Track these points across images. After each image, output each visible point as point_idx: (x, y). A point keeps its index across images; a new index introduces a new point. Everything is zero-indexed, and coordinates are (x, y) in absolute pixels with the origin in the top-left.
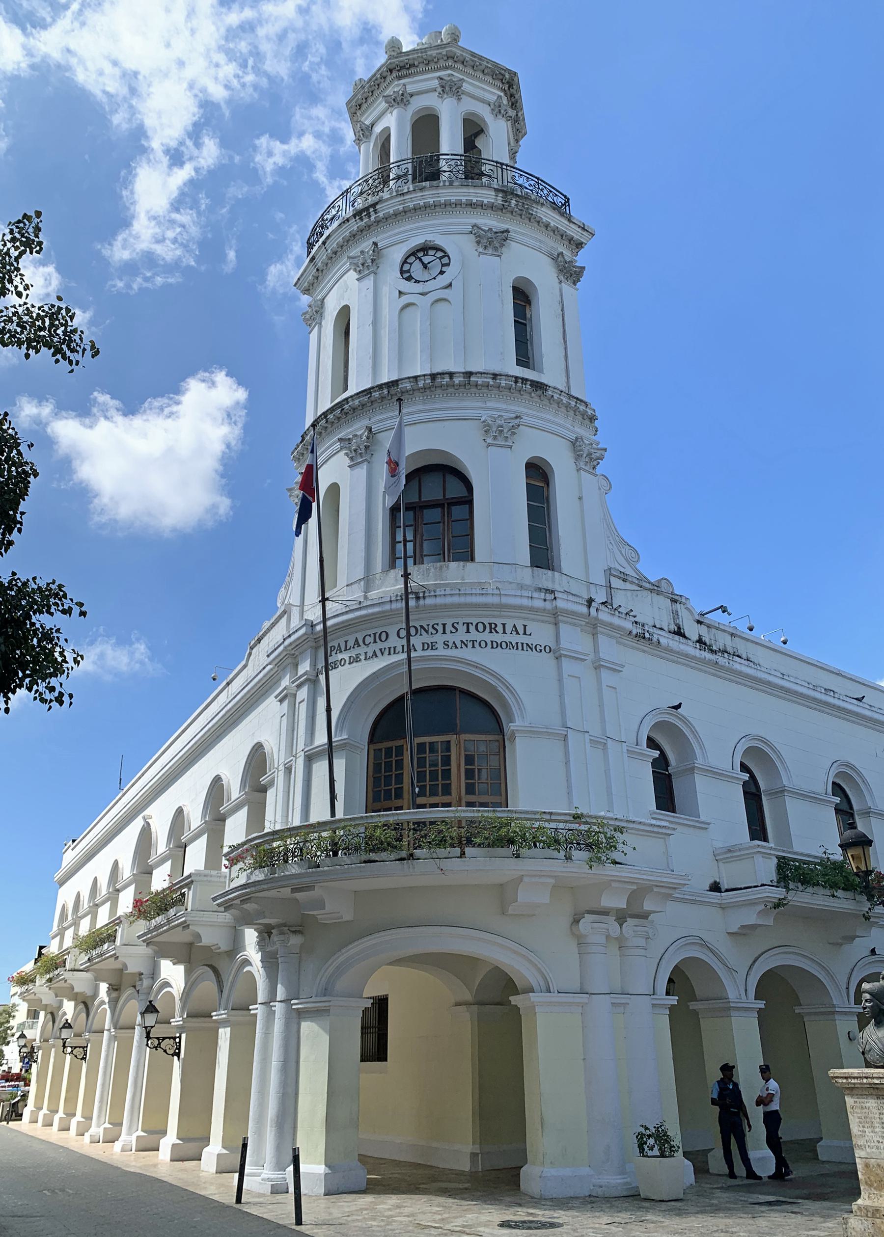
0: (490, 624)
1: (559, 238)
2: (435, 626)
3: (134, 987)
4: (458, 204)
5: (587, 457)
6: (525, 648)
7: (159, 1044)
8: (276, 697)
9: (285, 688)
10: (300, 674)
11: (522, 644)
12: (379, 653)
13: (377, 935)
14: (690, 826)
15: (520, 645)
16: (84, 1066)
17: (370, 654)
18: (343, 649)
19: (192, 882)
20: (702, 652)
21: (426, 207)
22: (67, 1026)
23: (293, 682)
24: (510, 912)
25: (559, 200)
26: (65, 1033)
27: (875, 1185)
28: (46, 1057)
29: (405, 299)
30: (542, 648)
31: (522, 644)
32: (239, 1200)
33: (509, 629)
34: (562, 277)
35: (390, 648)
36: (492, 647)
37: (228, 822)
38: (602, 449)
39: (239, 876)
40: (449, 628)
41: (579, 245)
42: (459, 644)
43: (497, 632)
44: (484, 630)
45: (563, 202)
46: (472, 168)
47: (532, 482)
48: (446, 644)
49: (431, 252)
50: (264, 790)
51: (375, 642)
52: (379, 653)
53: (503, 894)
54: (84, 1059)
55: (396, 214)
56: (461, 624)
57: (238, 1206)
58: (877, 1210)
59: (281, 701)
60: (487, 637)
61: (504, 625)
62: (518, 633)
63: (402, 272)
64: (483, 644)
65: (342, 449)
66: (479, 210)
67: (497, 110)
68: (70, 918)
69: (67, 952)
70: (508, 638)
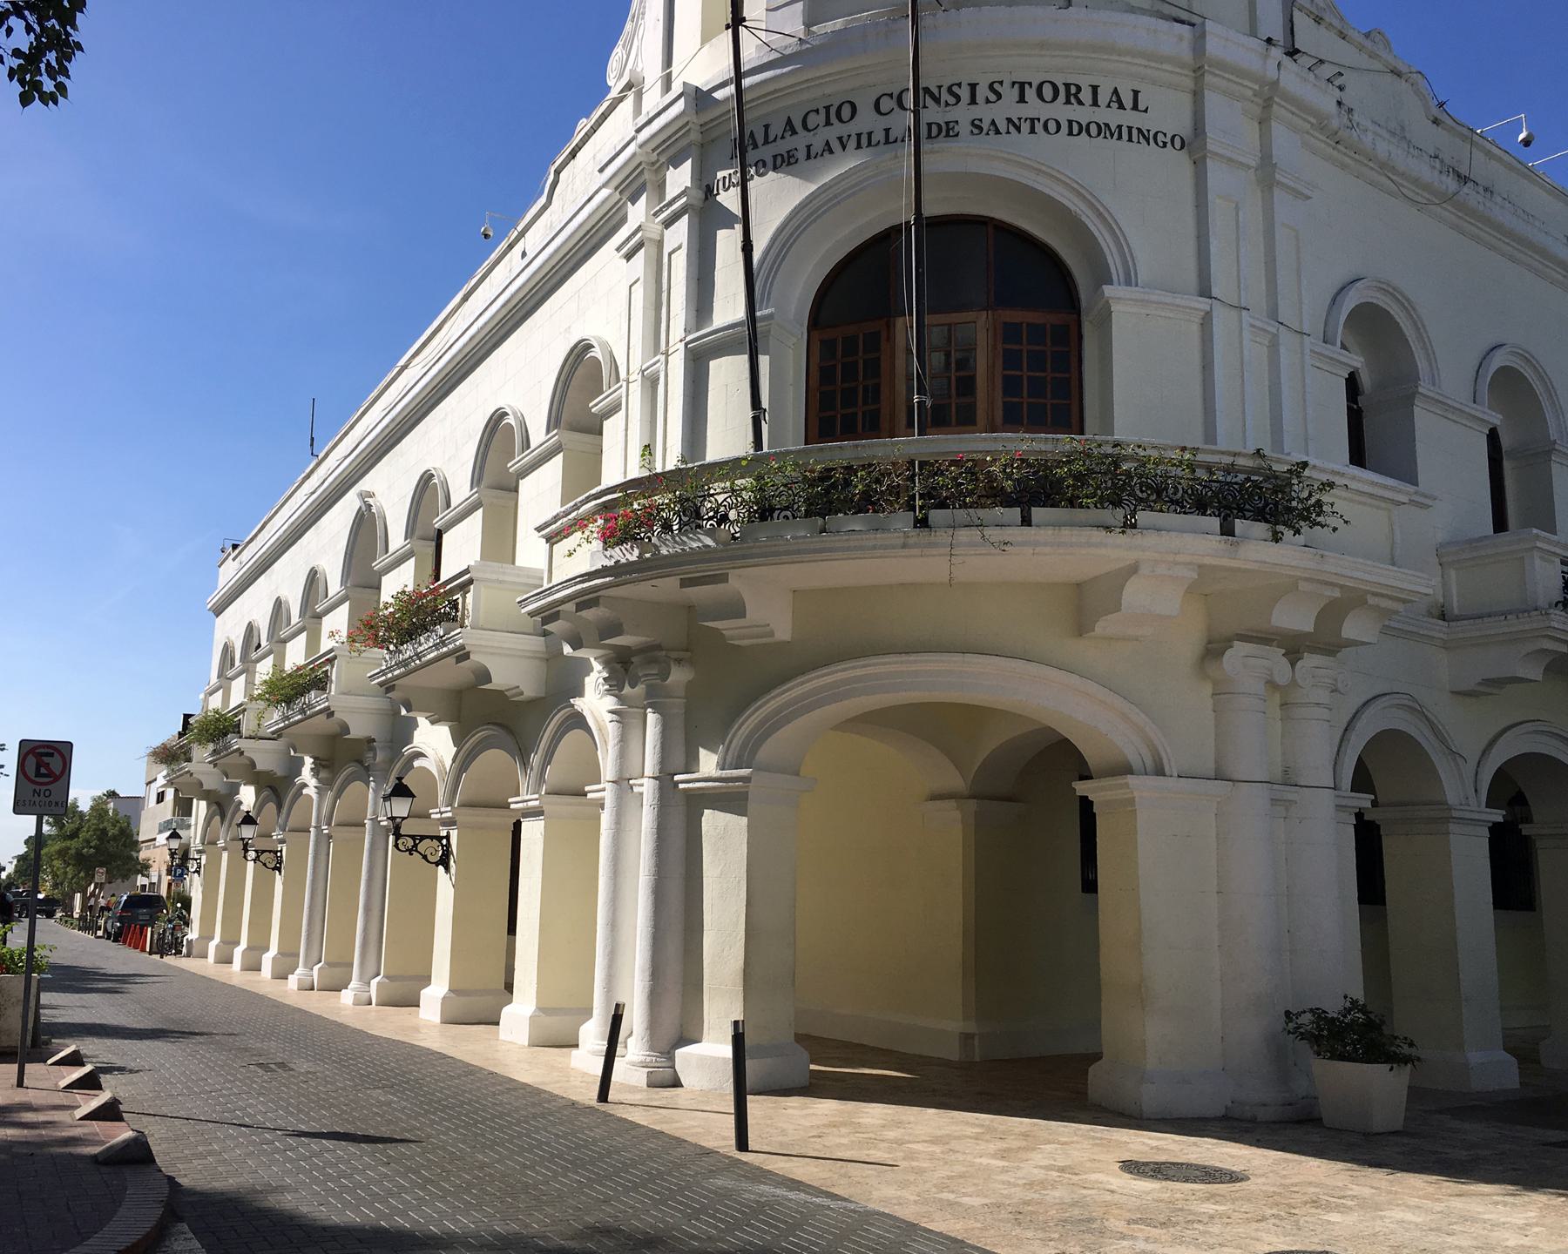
0: (1067, 86)
2: (955, 89)
3: (360, 762)
6: (1135, 138)
7: (415, 845)
8: (618, 250)
9: (639, 229)
10: (669, 198)
11: (1130, 129)
12: (835, 145)
17: (818, 146)
18: (760, 140)
19: (471, 581)
20: (1444, 178)
22: (248, 820)
23: (656, 215)
26: (248, 832)
28: (215, 863)
30: (1168, 140)
32: (603, 1095)
33: (1104, 97)
35: (859, 136)
36: (1070, 133)
37: (525, 485)
43: (1080, 103)
44: (1055, 98)
48: (976, 126)
51: (828, 123)
52: (835, 145)
54: (444, 862)
56: (1007, 84)
57: (602, 1107)
60: (1061, 111)
61: (1095, 89)
62: (1121, 106)
64: (1052, 126)
68: (237, 663)
69: (241, 709)
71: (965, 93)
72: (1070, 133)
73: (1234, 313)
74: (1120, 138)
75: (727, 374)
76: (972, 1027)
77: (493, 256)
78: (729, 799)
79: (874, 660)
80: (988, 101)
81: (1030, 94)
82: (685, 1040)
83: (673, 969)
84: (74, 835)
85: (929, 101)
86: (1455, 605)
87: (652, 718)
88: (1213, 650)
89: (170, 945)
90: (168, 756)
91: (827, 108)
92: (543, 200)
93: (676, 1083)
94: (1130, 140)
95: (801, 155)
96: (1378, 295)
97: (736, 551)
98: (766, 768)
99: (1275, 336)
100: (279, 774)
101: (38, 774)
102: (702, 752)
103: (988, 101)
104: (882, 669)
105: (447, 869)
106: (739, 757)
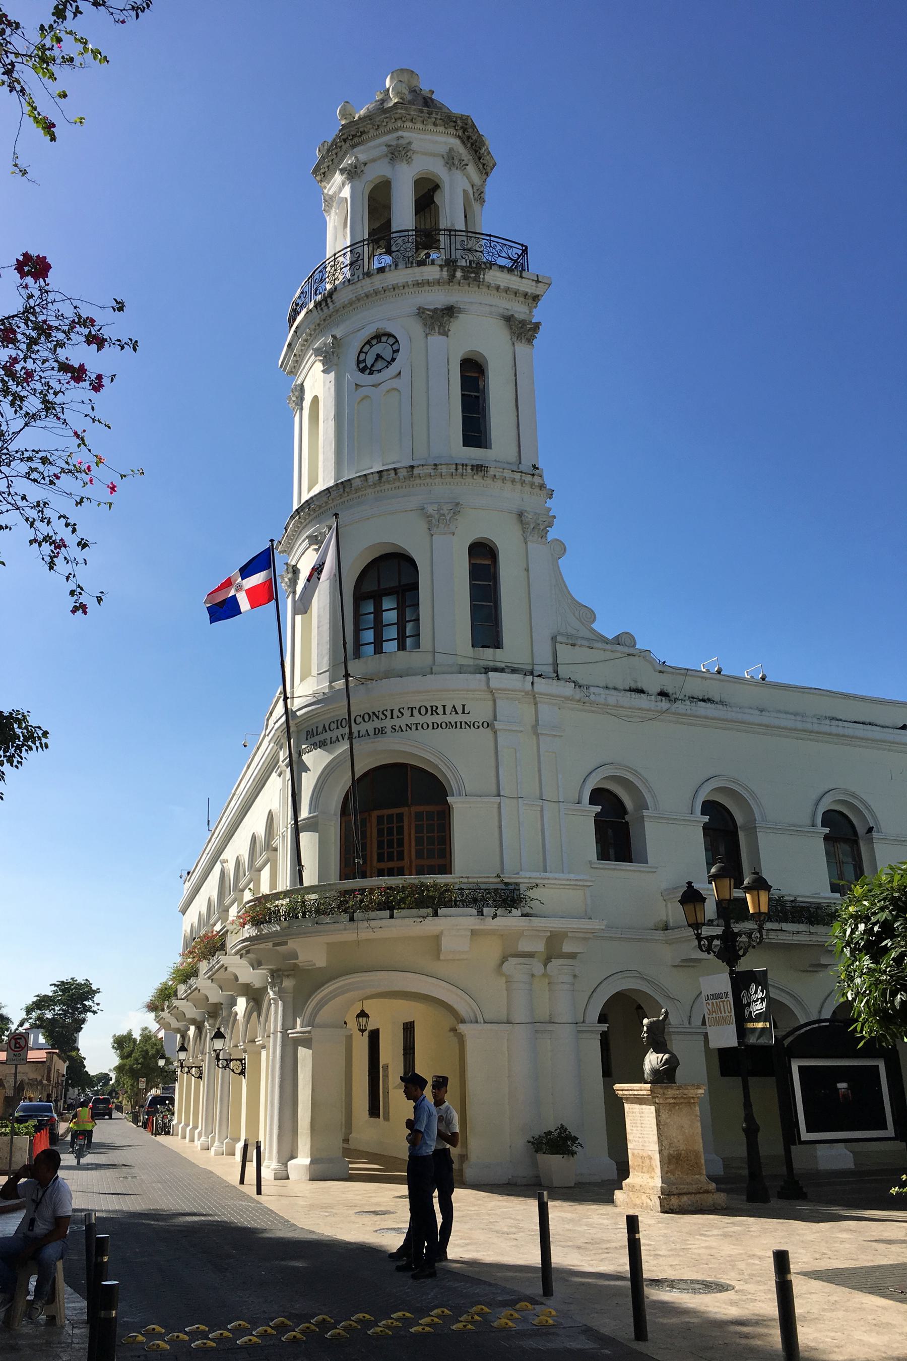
0: (432, 707)
1: (513, 296)
5: (533, 525)
12: (340, 738)
13: (359, 975)
14: (648, 872)
15: (458, 724)
16: (244, 1082)
17: (334, 739)
19: (227, 931)
20: (659, 704)
21: (376, 293)
25: (515, 252)
29: (363, 391)
34: (515, 339)
39: (249, 931)
40: (396, 713)
41: (536, 298)
45: (520, 252)
46: (427, 237)
47: (478, 562)
52: (340, 738)
54: (242, 1073)
55: (351, 303)
56: (406, 709)
60: (429, 719)
61: (444, 706)
62: (457, 713)
64: (425, 726)
65: (310, 545)
66: (426, 288)
70: (448, 718)
71: (388, 714)
73: (515, 801)
75: (308, 840)
78: (306, 1042)
79: (347, 977)
81: (416, 712)
82: (293, 1157)
84: (129, 1055)
85: (375, 718)
86: (671, 920)
87: (280, 1002)
88: (504, 959)
89: (165, 1130)
90: (153, 1007)
95: (328, 742)
98: (319, 1026)
101: (16, 1047)
104: (346, 982)
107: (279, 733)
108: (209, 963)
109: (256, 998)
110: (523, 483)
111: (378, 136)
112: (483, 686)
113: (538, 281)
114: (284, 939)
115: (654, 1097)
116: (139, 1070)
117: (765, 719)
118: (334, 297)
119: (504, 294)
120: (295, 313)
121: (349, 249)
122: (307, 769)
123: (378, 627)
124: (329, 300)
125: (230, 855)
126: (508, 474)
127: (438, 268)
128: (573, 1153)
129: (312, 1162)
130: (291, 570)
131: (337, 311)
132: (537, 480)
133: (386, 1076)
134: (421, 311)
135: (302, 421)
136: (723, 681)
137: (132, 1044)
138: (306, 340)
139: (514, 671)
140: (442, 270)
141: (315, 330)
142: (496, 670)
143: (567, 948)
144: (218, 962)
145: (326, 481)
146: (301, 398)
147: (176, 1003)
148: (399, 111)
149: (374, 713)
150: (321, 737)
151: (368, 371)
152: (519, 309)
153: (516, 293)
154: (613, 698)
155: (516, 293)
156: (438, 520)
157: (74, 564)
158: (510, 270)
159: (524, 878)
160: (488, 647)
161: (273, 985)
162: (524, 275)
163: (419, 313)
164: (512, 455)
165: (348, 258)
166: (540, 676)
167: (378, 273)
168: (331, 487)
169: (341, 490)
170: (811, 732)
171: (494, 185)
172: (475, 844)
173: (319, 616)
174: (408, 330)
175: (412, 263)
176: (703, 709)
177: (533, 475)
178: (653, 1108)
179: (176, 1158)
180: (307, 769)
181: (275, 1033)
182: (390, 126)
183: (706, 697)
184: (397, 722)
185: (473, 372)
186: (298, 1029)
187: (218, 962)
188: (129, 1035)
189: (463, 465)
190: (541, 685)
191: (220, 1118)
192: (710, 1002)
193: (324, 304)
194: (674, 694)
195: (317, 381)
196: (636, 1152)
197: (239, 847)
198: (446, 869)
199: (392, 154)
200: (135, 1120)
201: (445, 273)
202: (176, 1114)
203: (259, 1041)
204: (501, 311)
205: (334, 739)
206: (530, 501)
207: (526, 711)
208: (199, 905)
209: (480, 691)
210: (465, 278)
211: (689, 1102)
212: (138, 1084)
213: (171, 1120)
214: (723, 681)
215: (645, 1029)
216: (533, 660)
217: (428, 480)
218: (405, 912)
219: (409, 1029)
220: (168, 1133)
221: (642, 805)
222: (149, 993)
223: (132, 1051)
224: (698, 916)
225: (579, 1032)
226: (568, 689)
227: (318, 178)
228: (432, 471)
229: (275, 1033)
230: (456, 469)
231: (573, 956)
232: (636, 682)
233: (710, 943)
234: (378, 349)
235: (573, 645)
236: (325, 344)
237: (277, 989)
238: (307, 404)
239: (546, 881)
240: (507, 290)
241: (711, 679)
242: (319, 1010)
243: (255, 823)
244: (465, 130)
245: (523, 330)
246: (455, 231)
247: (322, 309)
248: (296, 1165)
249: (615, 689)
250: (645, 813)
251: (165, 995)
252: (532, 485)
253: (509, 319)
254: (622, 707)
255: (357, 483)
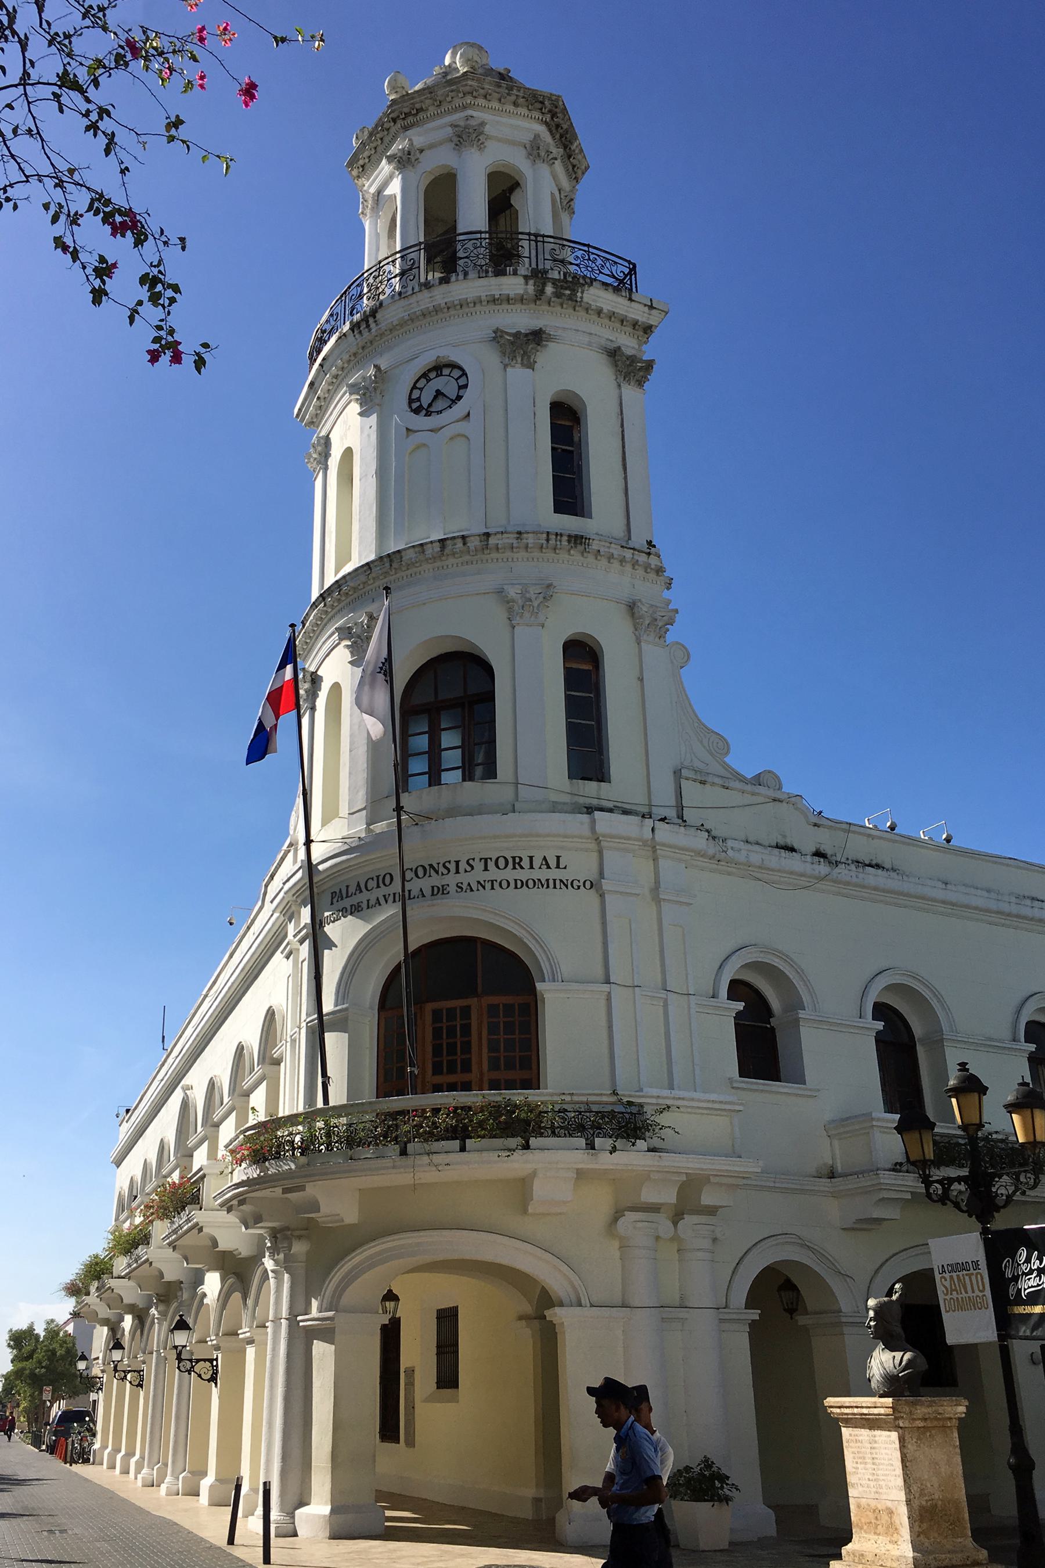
0: (514, 858)
1: (618, 325)
2: (447, 864)
4: (477, 302)
5: (649, 622)
6: (558, 886)
11: (554, 880)
12: (382, 901)
16: (215, 1392)
17: (372, 902)
19: (204, 1176)
20: (816, 866)
21: (437, 310)
24: (530, 1211)
25: (621, 270)
27: (865, 1527)
30: (581, 884)
31: (554, 880)
33: (537, 863)
36: (516, 887)
38: (673, 610)
39: (242, 1173)
40: (463, 866)
41: (648, 329)
42: (474, 886)
43: (522, 868)
45: (627, 271)
47: (574, 666)
49: (446, 371)
50: (277, 1062)
51: (378, 886)
52: (382, 901)
53: (521, 1191)
54: (213, 1379)
55: (403, 323)
56: (477, 860)
58: (862, 1555)
59: (288, 957)
60: (510, 874)
61: (531, 858)
62: (549, 867)
63: (411, 401)
65: (341, 639)
66: (505, 306)
67: (535, 152)
71: (452, 867)
72: (516, 887)
74: (548, 887)
75: (335, 1043)
76: (541, 1494)
77: (242, 932)
78: (326, 1333)
80: (466, 871)
81: (491, 865)
82: (303, 1503)
83: (296, 1452)
84: (30, 1356)
86: (839, 1165)
87: (286, 1276)
88: (617, 1215)
89: (84, 1457)
90: (74, 1290)
91: (378, 877)
92: (260, 903)
93: (296, 1535)
94: (555, 887)
95: (364, 905)
96: (762, 955)
97: (305, 1174)
98: (346, 1311)
99: (666, 1001)
100: (141, 1306)
102: (313, 1300)
103: (466, 871)
104: (402, 1242)
105: (216, 1384)
106: (331, 1303)
107: (289, 897)
108: (172, 1223)
109: (239, 1273)
110: (635, 564)
111: (439, 115)
112: (586, 831)
113: (651, 307)
114: (297, 1182)
115: (896, 1419)
116: (42, 1375)
117: (951, 896)
118: (378, 316)
119: (607, 321)
120: (322, 341)
121: (398, 255)
122: (331, 945)
123: (434, 753)
124: (371, 320)
125: (197, 1080)
126: (616, 550)
127: (522, 280)
128: (727, 1499)
129: (333, 1511)
130: (309, 678)
131: (382, 335)
132: (653, 561)
133: (410, 1384)
134: (498, 335)
135: (326, 489)
136: (895, 841)
137: (33, 1341)
138: (336, 377)
139: (626, 812)
140: (527, 284)
141: (349, 361)
142: (602, 810)
143: (707, 1199)
144: (188, 1220)
145: (362, 552)
146: (326, 455)
147: (112, 1283)
148: (470, 82)
149: (431, 866)
150: (354, 900)
151: (424, 412)
152: (628, 343)
153: (622, 321)
154: (757, 856)
155: (622, 321)
156: (523, 606)
157: (161, 244)
158: (616, 290)
159: (651, 1095)
160: (590, 780)
161: (274, 1251)
162: (634, 297)
163: (494, 338)
164: (617, 528)
165: (397, 266)
166: (663, 820)
167: (440, 283)
168: (372, 562)
169: (387, 565)
170: (1009, 915)
171: (585, 191)
172: (574, 1048)
173: (352, 736)
174: (479, 360)
175: (487, 272)
176: (872, 877)
177: (649, 554)
178: (894, 1435)
179: (110, 1502)
180: (331, 945)
181: (277, 1320)
182: (458, 102)
183: (874, 863)
184: (464, 878)
185: (566, 419)
186: (314, 1312)
187: (188, 1220)
188: (31, 1330)
189: (557, 534)
190: (664, 833)
191: (176, 1442)
192: (947, 1275)
193: (363, 326)
194: (834, 857)
195: (350, 428)
196: (863, 1502)
197: (216, 1063)
198: (532, 1082)
199: (459, 136)
200: (37, 1442)
201: (531, 288)
202: (99, 1436)
203: (245, 1332)
204: (603, 342)
205: (372, 902)
206: (647, 590)
207: (643, 868)
208: (146, 1150)
209: (581, 837)
210: (558, 295)
211: (940, 1425)
212: (41, 1393)
213: (92, 1444)
214: (895, 841)
215: (871, 1314)
216: (650, 800)
217: (509, 554)
218: (486, 1142)
219: (447, 1320)
220: (86, 1461)
221: (795, 1004)
222: (72, 1270)
223: (34, 1351)
224: (926, 1151)
225: (722, 1321)
226: (700, 841)
227: (355, 173)
228: (515, 541)
229: (277, 1320)
230: (548, 540)
231: (712, 1211)
232: (784, 836)
233: (946, 1191)
234: (438, 383)
235: (703, 783)
236: (364, 378)
237: (281, 1256)
238: (334, 462)
239: (679, 1103)
240: (611, 315)
241: (881, 838)
242: (344, 1290)
243: (244, 1027)
244: (554, 115)
245: (632, 369)
246: (543, 236)
247: (360, 332)
248: (308, 1515)
249: (757, 843)
250: (802, 1014)
251: (97, 1271)
252: (647, 567)
253: (614, 354)
254: (768, 869)
255: (410, 555)
